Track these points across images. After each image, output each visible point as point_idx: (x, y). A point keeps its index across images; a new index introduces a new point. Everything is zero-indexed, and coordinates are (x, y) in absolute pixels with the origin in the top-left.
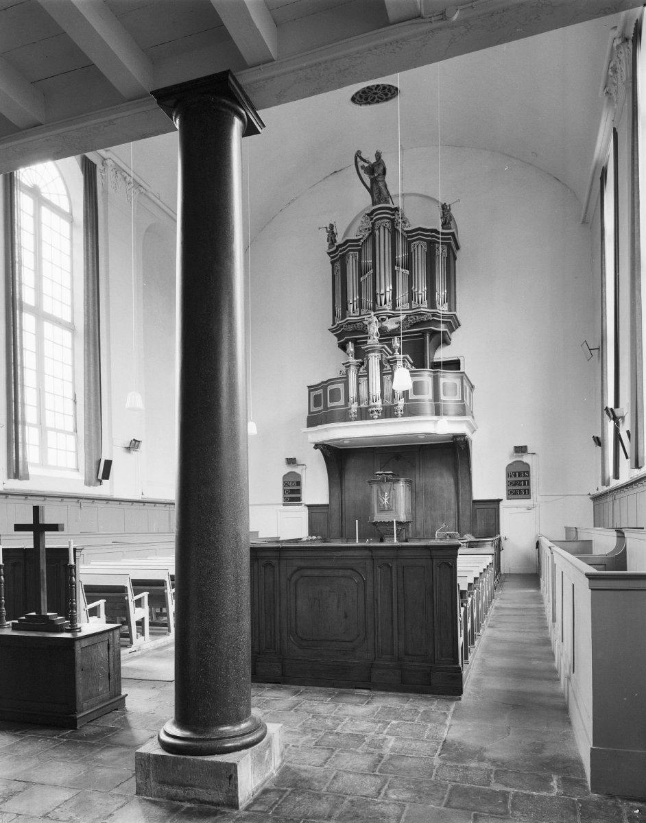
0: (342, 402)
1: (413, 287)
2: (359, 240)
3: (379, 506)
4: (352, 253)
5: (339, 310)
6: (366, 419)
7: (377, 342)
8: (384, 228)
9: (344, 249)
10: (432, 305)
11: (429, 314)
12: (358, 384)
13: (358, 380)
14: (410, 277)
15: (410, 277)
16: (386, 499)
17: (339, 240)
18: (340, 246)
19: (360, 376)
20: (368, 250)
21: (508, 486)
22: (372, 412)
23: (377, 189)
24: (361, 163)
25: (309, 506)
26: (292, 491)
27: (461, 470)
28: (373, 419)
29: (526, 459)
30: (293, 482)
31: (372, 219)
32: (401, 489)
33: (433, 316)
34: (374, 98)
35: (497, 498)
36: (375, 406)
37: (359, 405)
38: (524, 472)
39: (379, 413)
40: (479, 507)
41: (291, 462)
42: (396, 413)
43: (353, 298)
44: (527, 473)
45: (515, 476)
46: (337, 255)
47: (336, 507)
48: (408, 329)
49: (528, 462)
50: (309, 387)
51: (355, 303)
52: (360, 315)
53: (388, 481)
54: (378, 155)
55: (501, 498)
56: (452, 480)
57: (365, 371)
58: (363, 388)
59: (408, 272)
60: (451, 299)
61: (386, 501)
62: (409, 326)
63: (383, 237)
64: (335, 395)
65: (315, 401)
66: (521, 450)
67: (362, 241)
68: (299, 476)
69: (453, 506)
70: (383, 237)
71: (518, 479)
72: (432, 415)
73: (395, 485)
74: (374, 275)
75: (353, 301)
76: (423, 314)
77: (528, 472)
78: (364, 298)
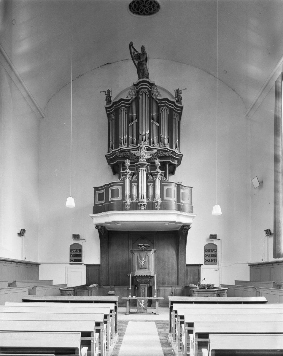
0: (120, 198)
1: (161, 134)
2: (129, 100)
3: (138, 266)
5: (113, 144)
7: (145, 161)
9: (118, 106)
11: (170, 152)
12: (131, 187)
14: (159, 128)
15: (159, 128)
16: (143, 262)
17: (113, 100)
18: (115, 103)
20: (134, 108)
21: (205, 257)
22: (141, 205)
23: (142, 71)
24: (133, 50)
25: (87, 265)
26: (76, 256)
27: (181, 245)
28: (141, 210)
29: (215, 242)
30: (77, 250)
31: (137, 88)
33: (172, 153)
34: (143, 10)
35: (199, 264)
36: (142, 202)
37: (131, 201)
38: (214, 250)
39: (145, 206)
41: (76, 237)
43: (123, 137)
45: (209, 251)
46: (113, 109)
47: (104, 266)
49: (216, 244)
50: (94, 188)
51: (125, 139)
52: (128, 147)
53: (144, 250)
54: (143, 48)
56: (174, 253)
57: (136, 179)
60: (179, 145)
61: (143, 263)
64: (114, 193)
65: (111, 192)
66: (213, 237)
67: (131, 101)
68: (81, 246)
71: (210, 253)
72: (176, 210)
73: (149, 253)
74: (138, 123)
75: (124, 138)
76: (166, 151)
77: (216, 250)
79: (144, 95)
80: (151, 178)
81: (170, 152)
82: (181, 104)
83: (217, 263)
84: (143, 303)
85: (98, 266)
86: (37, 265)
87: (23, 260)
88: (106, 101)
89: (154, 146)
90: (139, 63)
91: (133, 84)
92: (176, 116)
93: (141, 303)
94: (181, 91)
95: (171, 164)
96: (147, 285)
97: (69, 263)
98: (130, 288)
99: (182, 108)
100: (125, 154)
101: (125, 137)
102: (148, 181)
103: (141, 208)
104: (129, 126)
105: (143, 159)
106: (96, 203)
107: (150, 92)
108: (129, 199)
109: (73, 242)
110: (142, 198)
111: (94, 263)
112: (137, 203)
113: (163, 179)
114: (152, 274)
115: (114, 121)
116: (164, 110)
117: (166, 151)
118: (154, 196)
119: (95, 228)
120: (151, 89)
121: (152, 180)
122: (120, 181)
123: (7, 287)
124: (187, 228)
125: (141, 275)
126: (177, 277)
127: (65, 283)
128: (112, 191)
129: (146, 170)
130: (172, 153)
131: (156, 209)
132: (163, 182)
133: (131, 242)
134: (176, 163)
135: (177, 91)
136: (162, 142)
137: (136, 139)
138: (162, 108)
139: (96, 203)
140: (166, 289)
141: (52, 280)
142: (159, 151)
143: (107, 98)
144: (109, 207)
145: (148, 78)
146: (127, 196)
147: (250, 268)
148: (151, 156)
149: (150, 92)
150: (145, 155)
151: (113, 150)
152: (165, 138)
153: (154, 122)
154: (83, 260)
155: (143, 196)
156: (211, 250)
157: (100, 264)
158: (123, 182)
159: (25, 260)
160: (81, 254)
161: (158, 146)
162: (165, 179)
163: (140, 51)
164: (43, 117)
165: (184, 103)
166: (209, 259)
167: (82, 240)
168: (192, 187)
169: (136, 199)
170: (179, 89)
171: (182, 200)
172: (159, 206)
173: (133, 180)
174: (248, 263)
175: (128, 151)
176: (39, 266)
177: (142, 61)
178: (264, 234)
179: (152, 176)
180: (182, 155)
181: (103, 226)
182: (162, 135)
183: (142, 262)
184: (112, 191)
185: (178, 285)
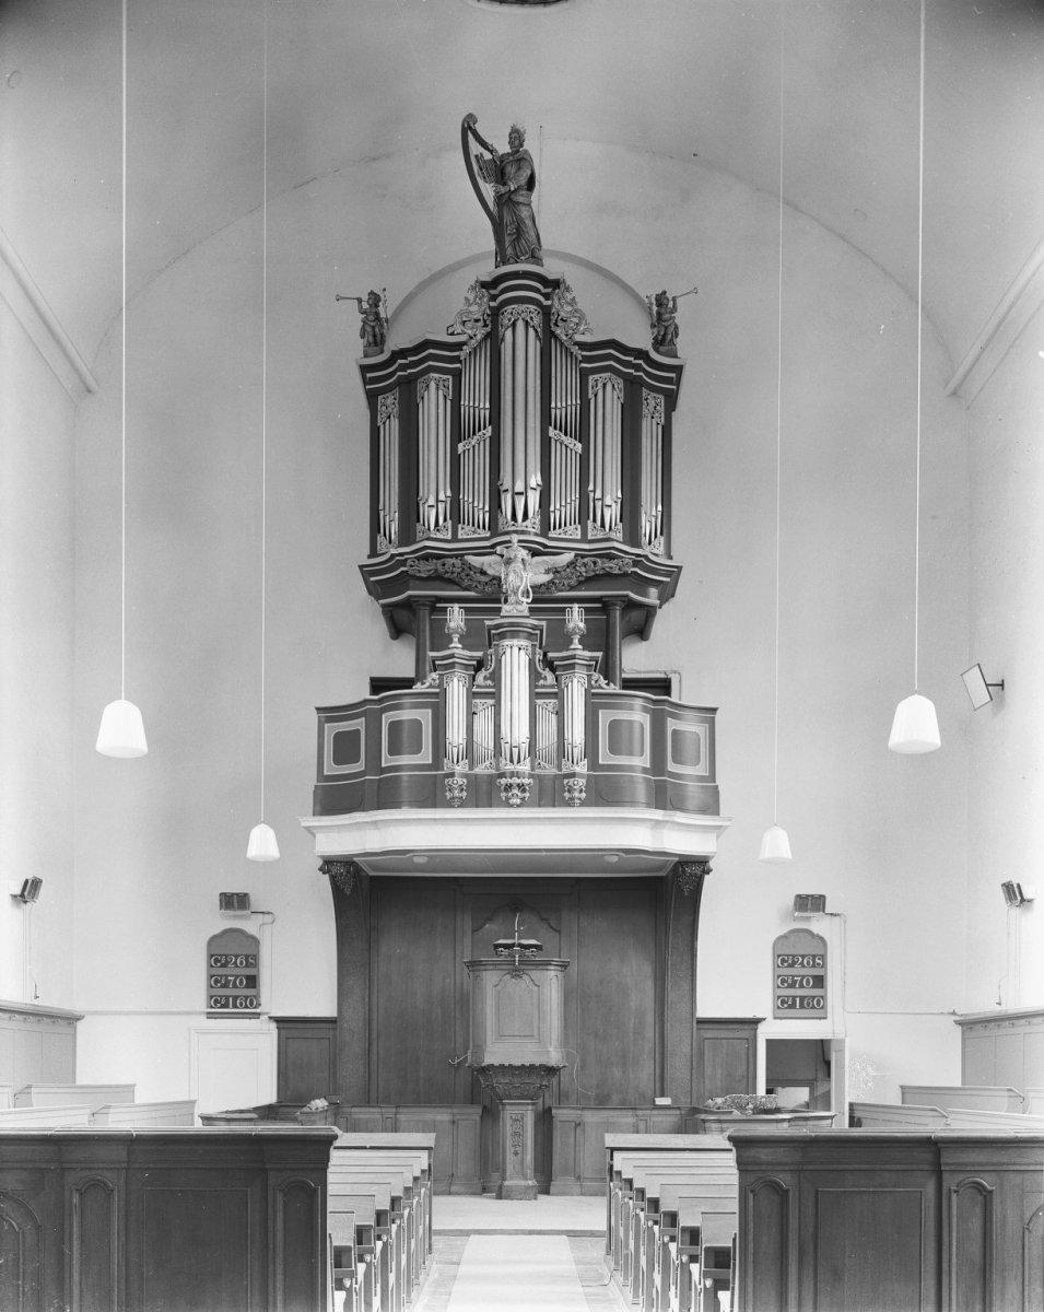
0: (425, 756)
1: (591, 487)
2: (459, 346)
4: (436, 375)
5: (392, 522)
6: (490, 805)
7: (526, 613)
8: (527, 323)
10: (633, 536)
12: (471, 714)
13: (469, 705)
18: (403, 353)
19: (554, 695)
22: (509, 787)
24: (475, 148)
25: (281, 1022)
29: (819, 924)
32: (551, 984)
33: (636, 564)
37: (471, 768)
39: (524, 791)
40: (709, 1035)
41: (234, 902)
42: (567, 795)
44: (818, 959)
47: (354, 1023)
48: (572, 588)
51: (441, 506)
52: (455, 539)
54: (516, 137)
55: (759, 1015)
56: (648, 969)
57: (489, 682)
58: (483, 725)
59: (579, 446)
62: (573, 582)
63: (522, 347)
66: (810, 903)
68: (255, 941)
69: (650, 1032)
70: (522, 347)
72: (648, 805)
74: (496, 443)
76: (611, 557)
77: (823, 957)
78: (466, 497)
79: (520, 325)
80: (550, 678)
81: (628, 559)
82: (675, 356)
83: (826, 1012)
85: (331, 1026)
86: (72, 1020)
87: (29, 1002)
88: (362, 336)
89: (562, 536)
90: (499, 198)
91: (477, 282)
92: (652, 403)
94: (674, 299)
95: (631, 605)
96: (533, 1104)
97: (204, 1013)
99: (678, 369)
100: (444, 565)
101: (442, 497)
102: (537, 690)
103: (507, 799)
104: (460, 450)
105: (519, 607)
106: (326, 773)
107: (546, 312)
108: (461, 763)
109: (221, 922)
110: (512, 761)
111: (311, 1013)
112: (490, 776)
113: (596, 681)
114: (554, 1057)
115: (395, 423)
116: (604, 385)
117: (611, 557)
118: (561, 750)
119: (320, 870)
120: (549, 303)
121: (552, 686)
122: (427, 690)
123: (9, 1107)
124: (697, 870)
126: (658, 1071)
127: (186, 1099)
128: (395, 727)
129: (530, 649)
130: (634, 561)
131: (569, 803)
132: (594, 694)
133: (466, 923)
134: (652, 597)
135: (656, 299)
136: (595, 521)
137: (487, 508)
138: (596, 376)
139: (326, 773)
140: (611, 1120)
141: (135, 1085)
142: (583, 557)
143: (369, 329)
144: (380, 794)
145: (535, 258)
146: (455, 750)
147: (963, 1032)
148: (551, 576)
149: (546, 312)
150: (523, 575)
151: (394, 551)
152: (608, 501)
153: (563, 437)
154: (263, 1000)
155: (515, 751)
157: (336, 1015)
158: (436, 695)
159: (36, 1002)
160: (255, 977)
161: (579, 537)
162: (603, 682)
163: (503, 147)
164: (89, 391)
165: (686, 347)
167: (261, 916)
168: (714, 710)
169: (487, 763)
170: (664, 293)
171: (676, 760)
172: (581, 791)
173: (478, 686)
175: (456, 556)
176: (78, 1023)
177: (516, 190)
178: (1001, 895)
179: (553, 670)
180: (679, 568)
181: (353, 863)
182: (594, 491)
184: (395, 727)
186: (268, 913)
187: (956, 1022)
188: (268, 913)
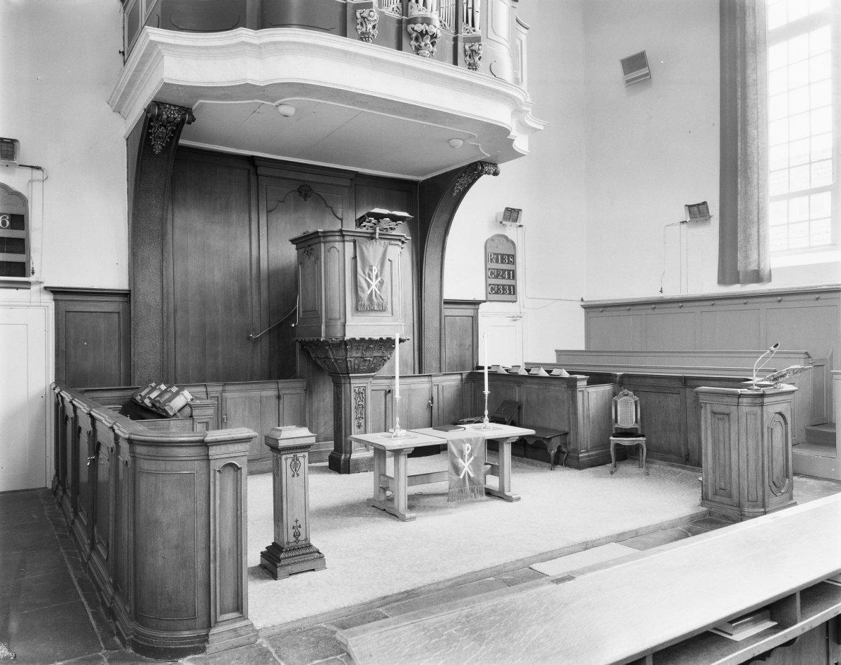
3: (357, 297)
21: (487, 277)
38: (508, 255)
44: (510, 258)
45: (497, 261)
77: (513, 256)
84: (470, 455)
93: (462, 457)
98: (487, 392)
125: (367, 338)
140: (412, 386)
156: (502, 255)
166: (498, 285)
167: (29, 171)
174: (582, 300)
183: (369, 285)
185: (420, 372)
186: (38, 168)
187: (581, 306)
188: (38, 168)
